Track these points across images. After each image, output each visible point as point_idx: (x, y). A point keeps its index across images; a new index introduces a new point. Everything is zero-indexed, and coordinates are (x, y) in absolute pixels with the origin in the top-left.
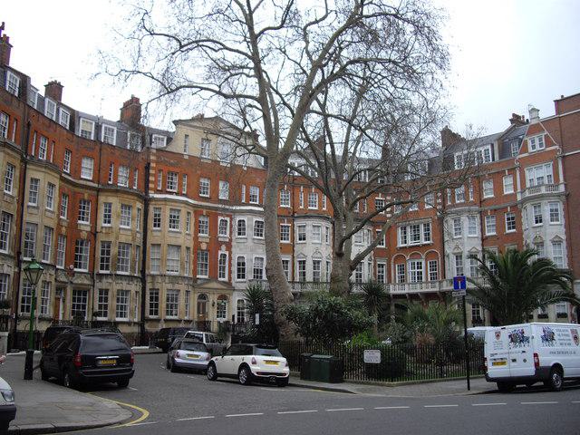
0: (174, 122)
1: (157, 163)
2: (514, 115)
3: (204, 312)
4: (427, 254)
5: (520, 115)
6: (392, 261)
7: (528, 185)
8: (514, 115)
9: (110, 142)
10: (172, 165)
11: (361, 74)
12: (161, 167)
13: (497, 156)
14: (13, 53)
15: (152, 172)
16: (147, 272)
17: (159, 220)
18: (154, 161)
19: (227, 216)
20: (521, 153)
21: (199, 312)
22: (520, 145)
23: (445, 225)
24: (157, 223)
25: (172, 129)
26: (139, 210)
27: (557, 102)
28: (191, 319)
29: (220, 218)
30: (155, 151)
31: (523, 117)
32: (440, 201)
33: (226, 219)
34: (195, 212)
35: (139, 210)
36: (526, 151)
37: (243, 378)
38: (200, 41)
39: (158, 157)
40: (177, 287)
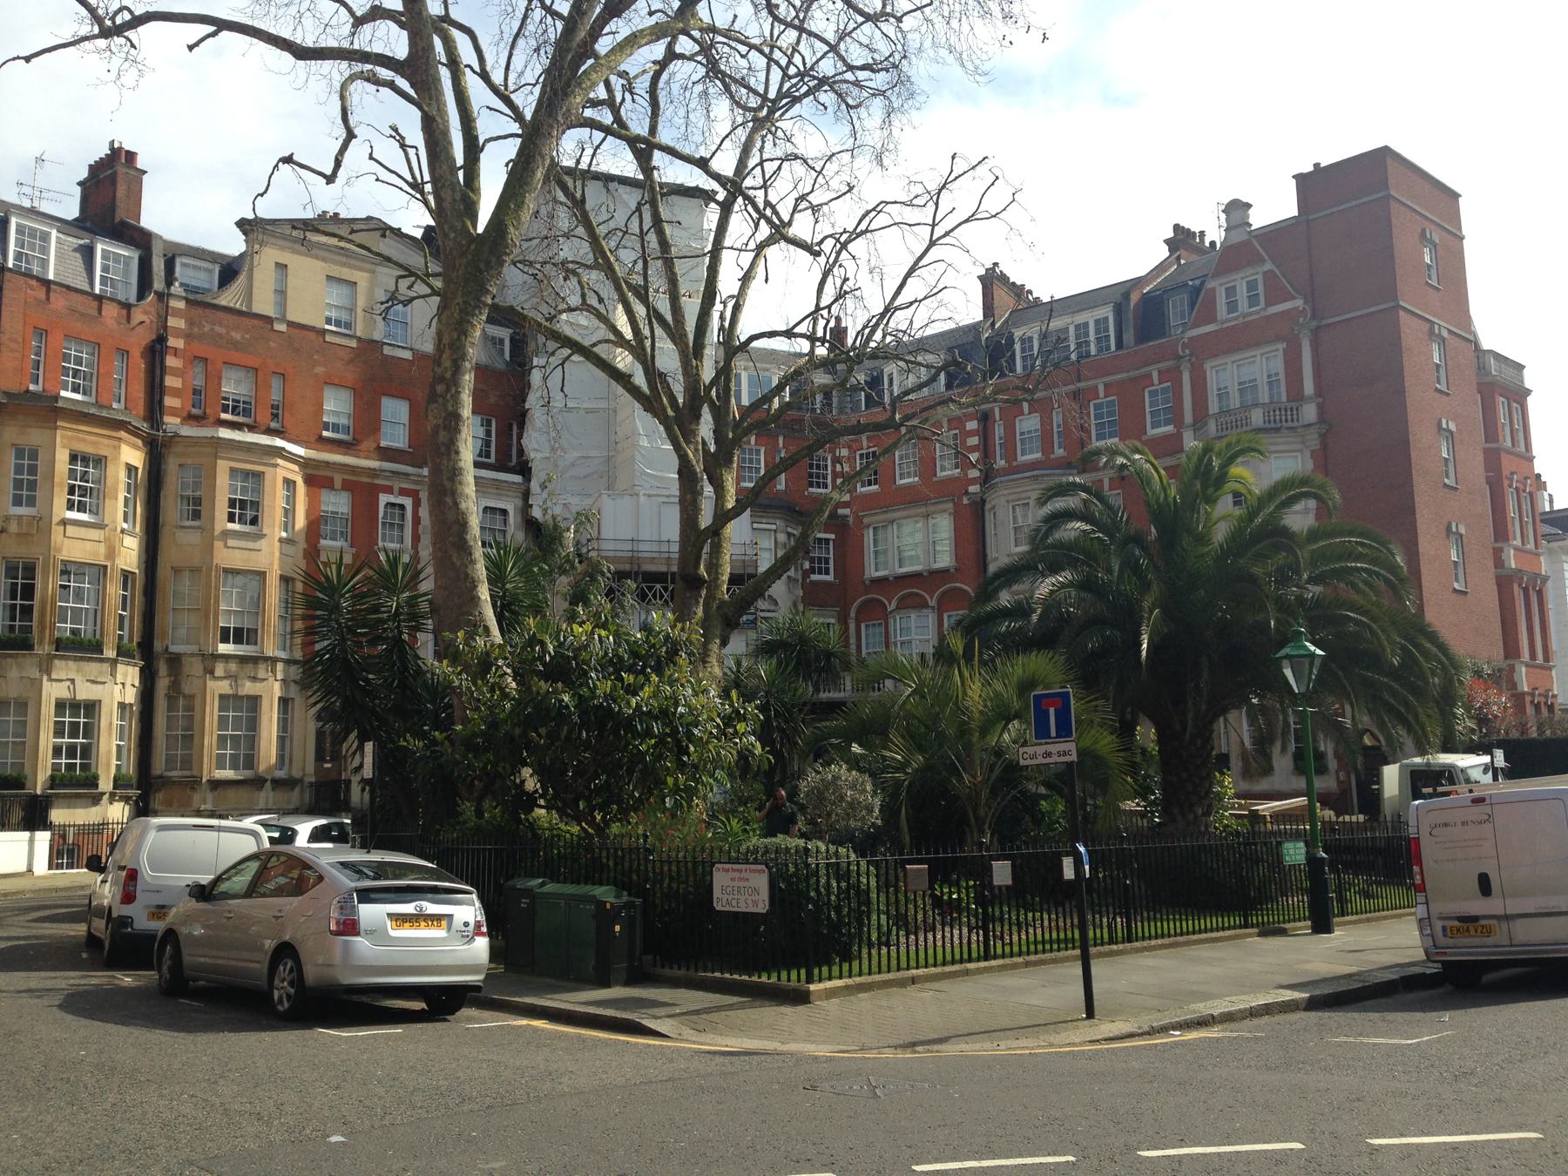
0: (242, 224)
1: (188, 337)
2: (1177, 227)
3: (336, 757)
4: (943, 594)
5: (1196, 229)
6: (853, 614)
7: (1213, 407)
8: (1177, 227)
9: (36, 269)
10: (235, 345)
11: (757, 82)
12: (201, 349)
13: (1129, 336)
14: (149, 186)
15: (171, 361)
16: (158, 646)
17: (32, 485)
18: (178, 333)
19: (403, 492)
20: (1196, 325)
21: (320, 758)
22: (1192, 305)
23: (989, 517)
24: (197, 509)
25: (234, 245)
26: (131, 469)
27: (1300, 179)
28: (296, 774)
29: (384, 499)
30: (181, 305)
31: (1202, 233)
32: (973, 441)
33: (400, 500)
34: (310, 481)
35: (131, 469)
36: (1212, 319)
37: (282, 990)
38: (669, 264)
39: (191, 323)
40: (248, 688)
